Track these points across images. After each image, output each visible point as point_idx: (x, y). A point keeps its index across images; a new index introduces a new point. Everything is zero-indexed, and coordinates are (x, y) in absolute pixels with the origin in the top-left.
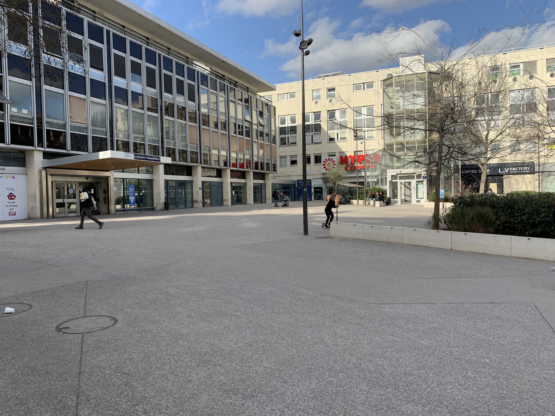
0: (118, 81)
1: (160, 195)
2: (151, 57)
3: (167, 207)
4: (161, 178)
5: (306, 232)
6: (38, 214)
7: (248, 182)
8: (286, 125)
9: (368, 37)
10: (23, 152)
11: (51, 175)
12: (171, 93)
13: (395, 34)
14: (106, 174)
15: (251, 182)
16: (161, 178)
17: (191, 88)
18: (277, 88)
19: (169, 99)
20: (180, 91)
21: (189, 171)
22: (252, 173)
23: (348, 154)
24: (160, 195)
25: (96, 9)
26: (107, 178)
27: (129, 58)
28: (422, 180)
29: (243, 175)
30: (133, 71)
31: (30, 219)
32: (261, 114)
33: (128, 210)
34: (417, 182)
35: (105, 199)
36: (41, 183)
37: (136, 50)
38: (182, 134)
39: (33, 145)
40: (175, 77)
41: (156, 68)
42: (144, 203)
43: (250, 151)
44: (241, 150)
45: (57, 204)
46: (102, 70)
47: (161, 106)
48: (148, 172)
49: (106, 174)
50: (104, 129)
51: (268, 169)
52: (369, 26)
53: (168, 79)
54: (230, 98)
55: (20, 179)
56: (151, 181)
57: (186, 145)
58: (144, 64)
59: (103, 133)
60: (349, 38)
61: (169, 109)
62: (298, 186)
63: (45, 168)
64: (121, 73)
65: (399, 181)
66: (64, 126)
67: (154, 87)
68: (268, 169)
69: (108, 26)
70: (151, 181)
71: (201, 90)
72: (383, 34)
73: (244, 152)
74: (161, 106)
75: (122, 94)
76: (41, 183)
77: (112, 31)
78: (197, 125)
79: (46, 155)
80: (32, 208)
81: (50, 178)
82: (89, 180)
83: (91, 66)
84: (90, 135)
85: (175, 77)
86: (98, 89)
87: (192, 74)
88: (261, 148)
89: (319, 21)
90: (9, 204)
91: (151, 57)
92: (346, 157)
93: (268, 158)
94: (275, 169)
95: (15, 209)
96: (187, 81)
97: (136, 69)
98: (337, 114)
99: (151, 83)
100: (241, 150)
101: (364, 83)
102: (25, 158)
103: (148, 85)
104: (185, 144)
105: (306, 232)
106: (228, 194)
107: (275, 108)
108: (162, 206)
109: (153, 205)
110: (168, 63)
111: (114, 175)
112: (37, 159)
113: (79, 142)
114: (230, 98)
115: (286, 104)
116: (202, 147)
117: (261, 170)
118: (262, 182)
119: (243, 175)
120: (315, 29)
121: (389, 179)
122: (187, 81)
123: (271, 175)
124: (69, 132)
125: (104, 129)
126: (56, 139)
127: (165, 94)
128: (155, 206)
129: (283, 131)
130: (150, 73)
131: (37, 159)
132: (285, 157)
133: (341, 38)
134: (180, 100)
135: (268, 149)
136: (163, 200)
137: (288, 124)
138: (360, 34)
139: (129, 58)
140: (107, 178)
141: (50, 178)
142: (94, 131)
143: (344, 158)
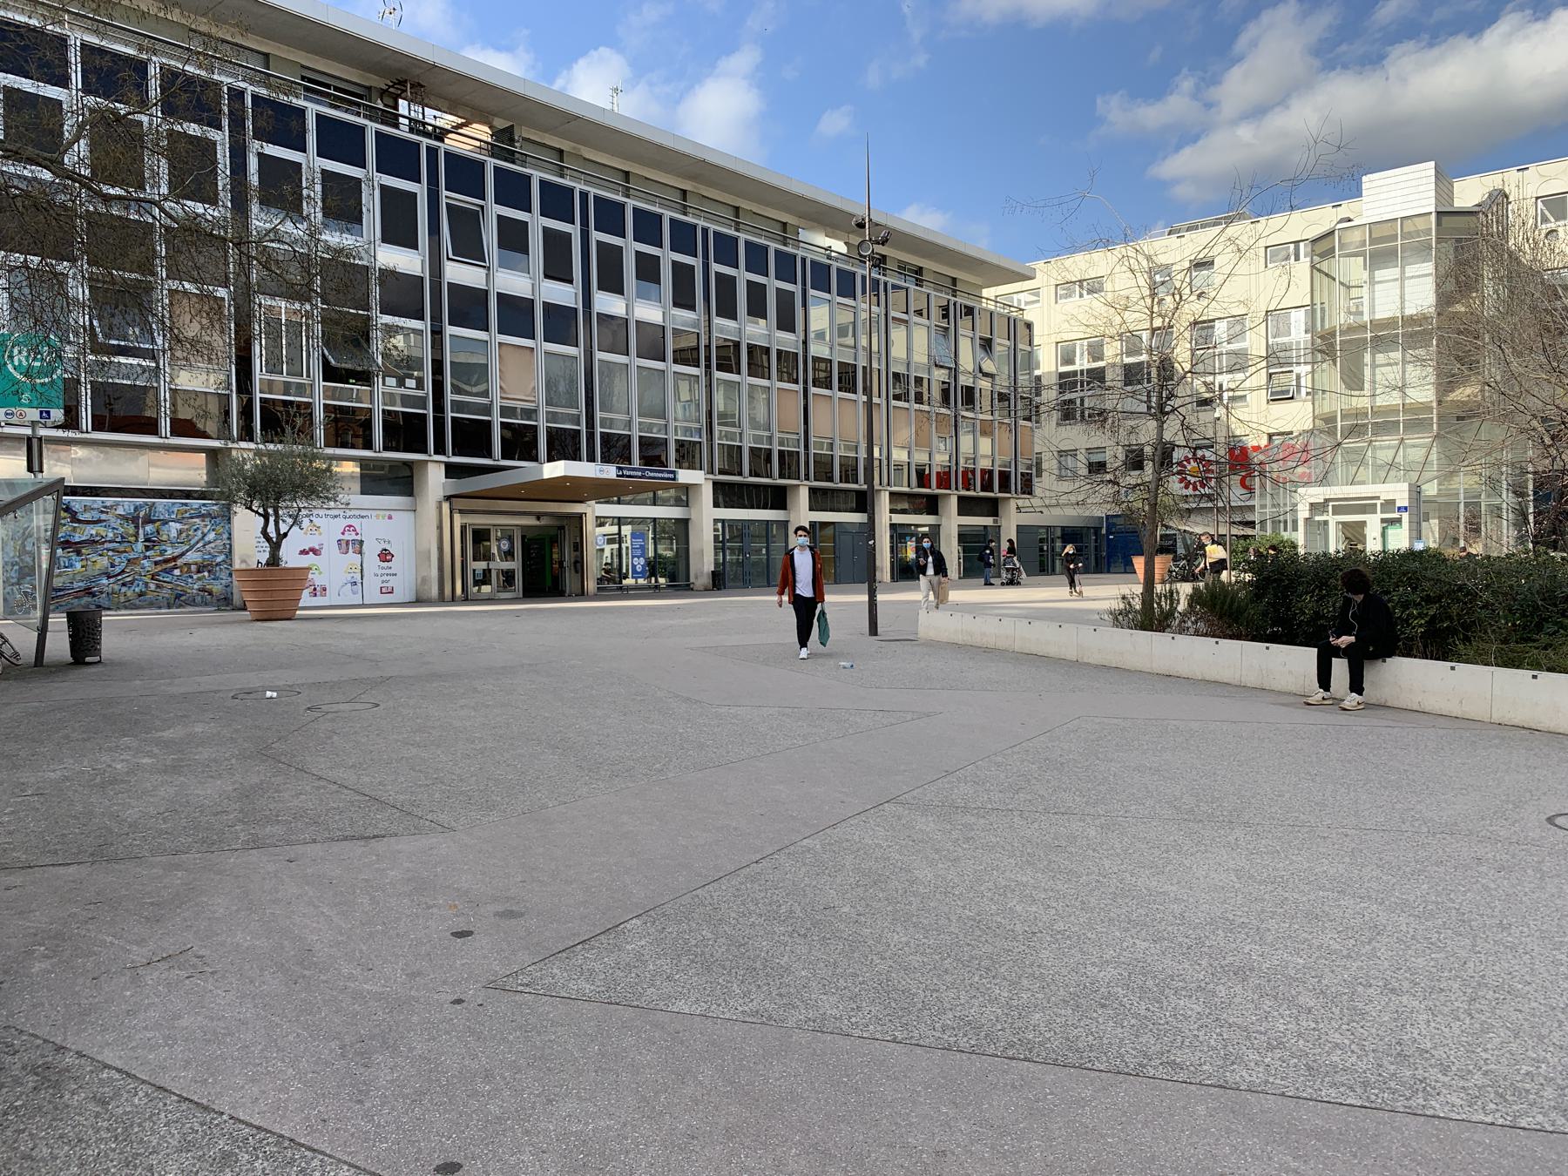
0: (607, 303)
1: (704, 557)
2: (684, 237)
3: (719, 581)
4: (707, 516)
5: (873, 630)
6: (435, 592)
7: (944, 522)
8: (1076, 367)
9: (1436, 52)
10: (408, 464)
11: (461, 512)
12: (733, 317)
13: (1538, 26)
14: (577, 508)
15: (952, 522)
16: (707, 516)
17: (785, 299)
18: (1039, 275)
19: (728, 333)
20: (757, 309)
21: (779, 498)
22: (954, 501)
23: (1251, 442)
24: (704, 557)
25: (565, 145)
26: (579, 518)
27: (631, 247)
28: (1396, 515)
29: (931, 505)
30: (640, 276)
31: (419, 601)
32: (987, 345)
33: (629, 588)
34: (1383, 521)
35: (576, 562)
36: (440, 527)
37: (648, 227)
38: (762, 412)
39: (425, 451)
40: (743, 276)
41: (695, 262)
42: (670, 573)
43: (950, 443)
44: (921, 441)
45: (470, 572)
46: (571, 282)
47: (708, 347)
48: (678, 502)
49: (577, 508)
50: (574, 411)
51: (1005, 486)
52: (1441, 13)
53: (727, 284)
54: (893, 314)
55: (404, 519)
56: (684, 523)
57: (770, 438)
58: (668, 257)
59: (571, 417)
60: (1373, 61)
61: (728, 357)
62: (1109, 532)
63: (448, 498)
64: (613, 284)
65: (1333, 520)
66: (487, 410)
67: (692, 308)
68: (1005, 486)
69: (587, 183)
70: (684, 523)
71: (810, 300)
72: (1492, 36)
73: (930, 446)
74: (708, 347)
75: (616, 331)
76: (440, 527)
77: (593, 191)
78: (799, 387)
79: (452, 471)
80: (424, 580)
81: (457, 516)
82: (544, 522)
83: (547, 276)
84: (543, 425)
85: (743, 276)
86: (560, 323)
87: (787, 268)
88: (984, 433)
89: (1266, 17)
90: (380, 572)
91: (684, 237)
92: (1244, 450)
93: (1007, 459)
94: (1027, 488)
95: (393, 582)
96: (773, 284)
97: (648, 269)
98: (1221, 329)
99: (683, 299)
100: (921, 441)
101: (1297, 243)
102: (412, 476)
103: (676, 304)
104: (766, 434)
105: (873, 630)
106: (951, 551)
107: (1029, 326)
108: (705, 580)
109: (688, 578)
110: (722, 244)
111: (593, 510)
112: (435, 480)
113: (521, 443)
114: (893, 314)
115: (1068, 310)
116: (812, 439)
117: (985, 492)
118: (988, 521)
119: (931, 505)
120: (1254, 44)
121: (1303, 513)
122: (773, 284)
123: (1013, 504)
124: (497, 420)
125: (574, 411)
126: (472, 437)
127: (718, 321)
128: (692, 580)
129: (1067, 382)
130: (683, 275)
131: (435, 480)
132: (1073, 453)
133: (1345, 67)
134: (756, 331)
135: (1006, 439)
136: (709, 566)
137: (1082, 363)
138: (1409, 45)
139: (631, 247)
140: (579, 518)
141: (457, 516)
142: (552, 417)
143: (1237, 452)
